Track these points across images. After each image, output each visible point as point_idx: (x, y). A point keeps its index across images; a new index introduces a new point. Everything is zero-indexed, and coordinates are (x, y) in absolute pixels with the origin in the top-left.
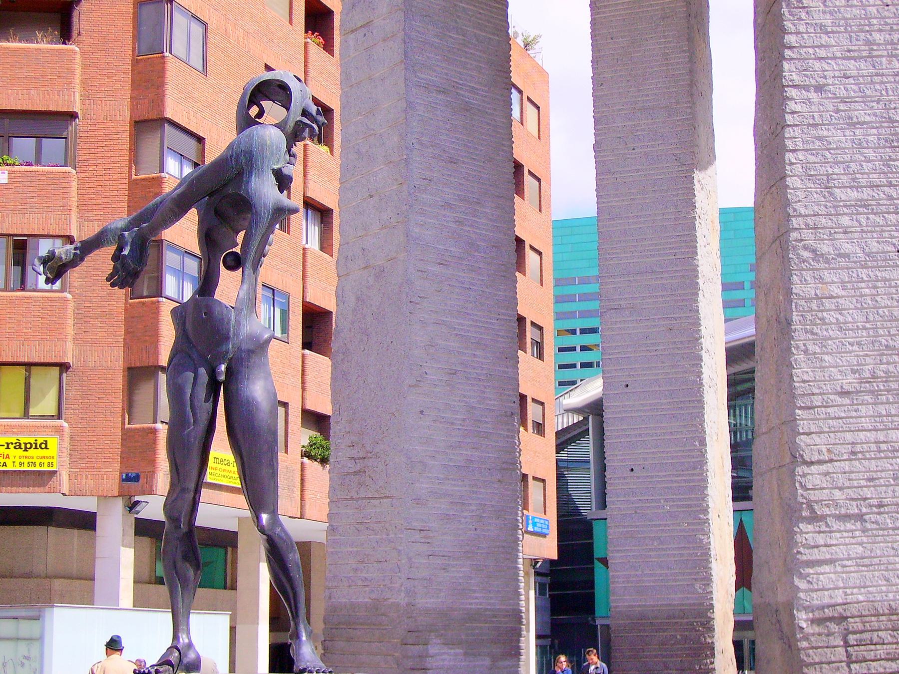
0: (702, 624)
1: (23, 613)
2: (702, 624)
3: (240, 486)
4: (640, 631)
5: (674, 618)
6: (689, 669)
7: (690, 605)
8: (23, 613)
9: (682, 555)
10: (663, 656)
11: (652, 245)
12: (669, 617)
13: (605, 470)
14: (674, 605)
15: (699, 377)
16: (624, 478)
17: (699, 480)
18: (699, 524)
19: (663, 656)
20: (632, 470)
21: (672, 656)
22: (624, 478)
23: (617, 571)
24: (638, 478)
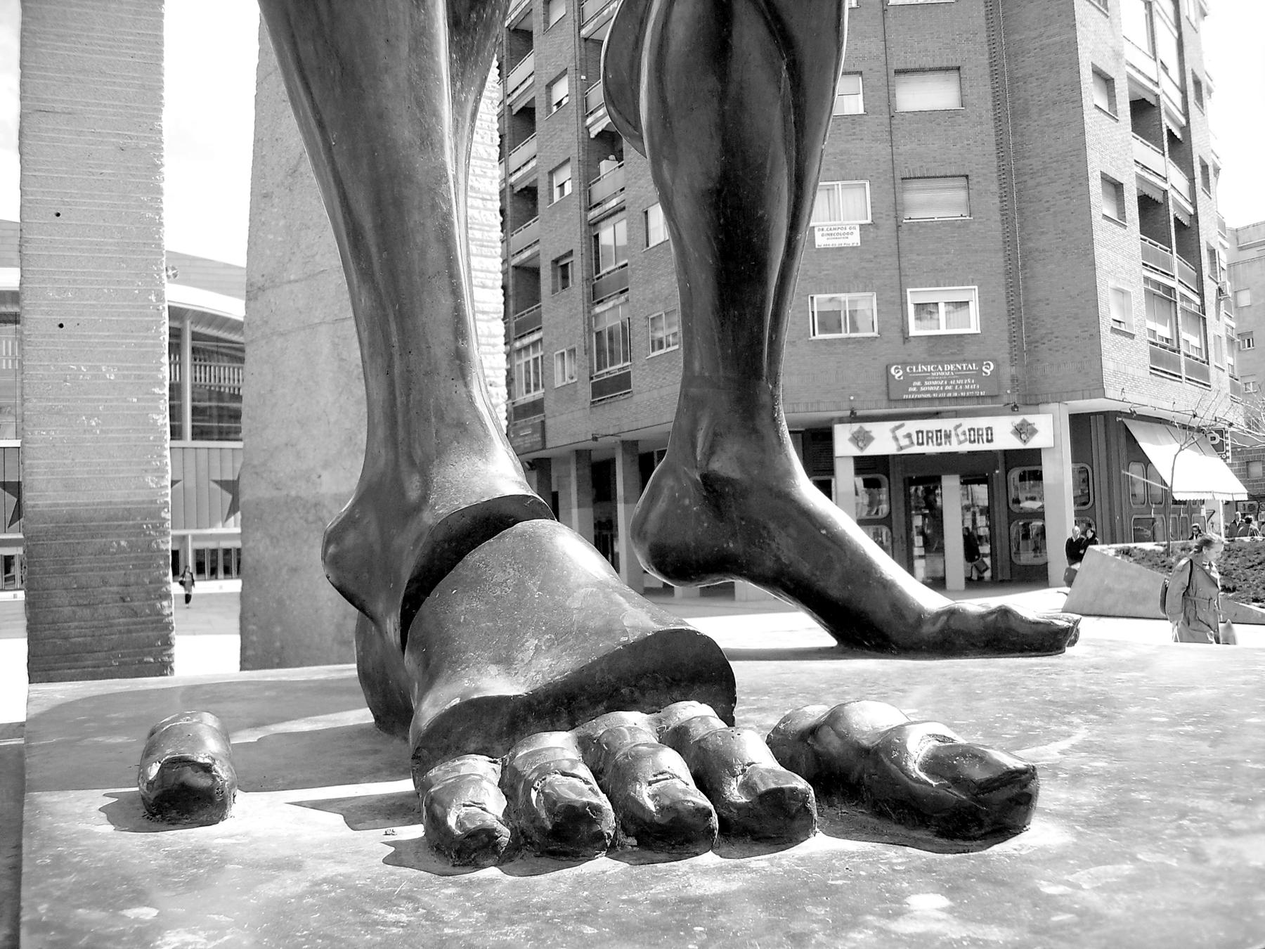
0: (154, 527)
1: (817, 166)
2: (154, 527)
3: (625, 222)
4: (69, 537)
5: (117, 520)
6: (137, 584)
7: (139, 503)
8: (817, 166)
9: (128, 439)
10: (101, 569)
11: (102, 39)
12: (109, 519)
13: (502, 223)
14: (116, 504)
15: (159, 214)
16: (51, 336)
17: (154, 345)
18: (153, 400)
19: (101, 569)
20: (61, 326)
21: (114, 568)
22: (51, 336)
23: (34, 458)
24: (70, 336)
